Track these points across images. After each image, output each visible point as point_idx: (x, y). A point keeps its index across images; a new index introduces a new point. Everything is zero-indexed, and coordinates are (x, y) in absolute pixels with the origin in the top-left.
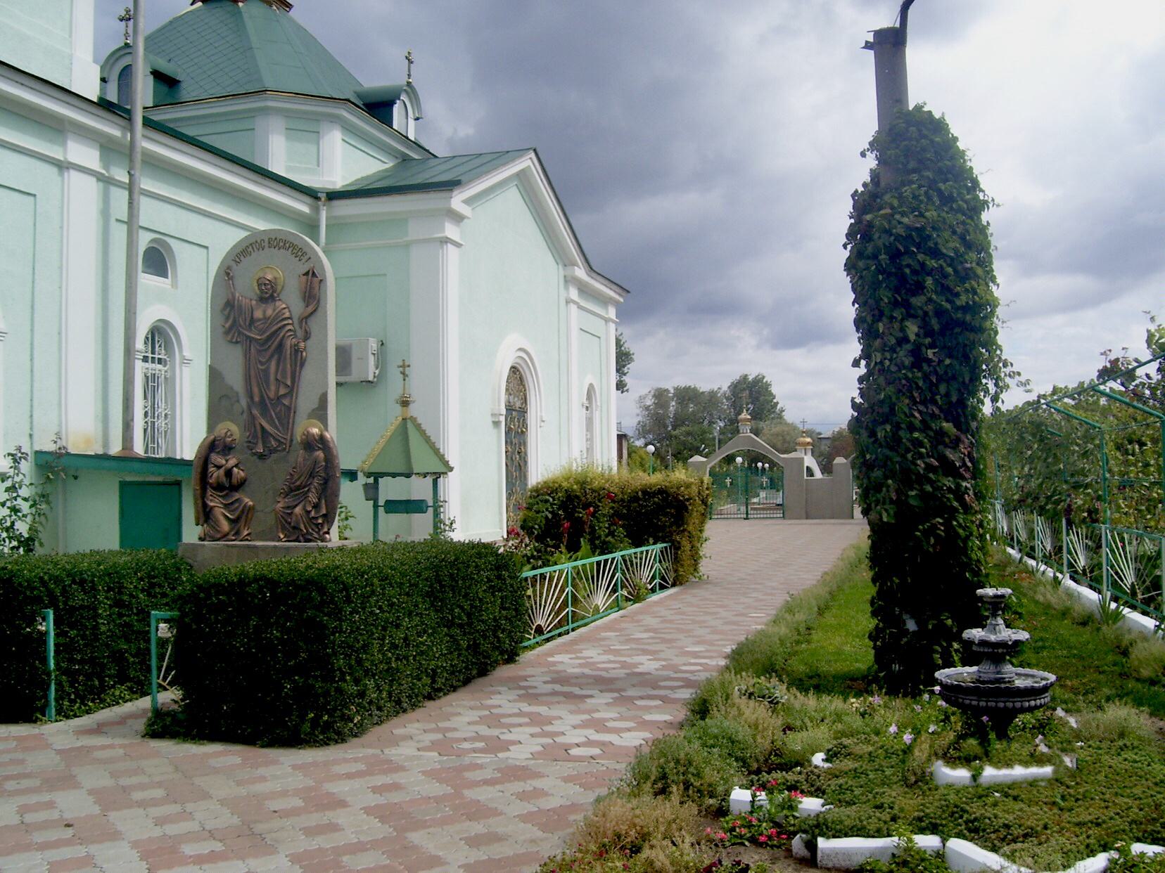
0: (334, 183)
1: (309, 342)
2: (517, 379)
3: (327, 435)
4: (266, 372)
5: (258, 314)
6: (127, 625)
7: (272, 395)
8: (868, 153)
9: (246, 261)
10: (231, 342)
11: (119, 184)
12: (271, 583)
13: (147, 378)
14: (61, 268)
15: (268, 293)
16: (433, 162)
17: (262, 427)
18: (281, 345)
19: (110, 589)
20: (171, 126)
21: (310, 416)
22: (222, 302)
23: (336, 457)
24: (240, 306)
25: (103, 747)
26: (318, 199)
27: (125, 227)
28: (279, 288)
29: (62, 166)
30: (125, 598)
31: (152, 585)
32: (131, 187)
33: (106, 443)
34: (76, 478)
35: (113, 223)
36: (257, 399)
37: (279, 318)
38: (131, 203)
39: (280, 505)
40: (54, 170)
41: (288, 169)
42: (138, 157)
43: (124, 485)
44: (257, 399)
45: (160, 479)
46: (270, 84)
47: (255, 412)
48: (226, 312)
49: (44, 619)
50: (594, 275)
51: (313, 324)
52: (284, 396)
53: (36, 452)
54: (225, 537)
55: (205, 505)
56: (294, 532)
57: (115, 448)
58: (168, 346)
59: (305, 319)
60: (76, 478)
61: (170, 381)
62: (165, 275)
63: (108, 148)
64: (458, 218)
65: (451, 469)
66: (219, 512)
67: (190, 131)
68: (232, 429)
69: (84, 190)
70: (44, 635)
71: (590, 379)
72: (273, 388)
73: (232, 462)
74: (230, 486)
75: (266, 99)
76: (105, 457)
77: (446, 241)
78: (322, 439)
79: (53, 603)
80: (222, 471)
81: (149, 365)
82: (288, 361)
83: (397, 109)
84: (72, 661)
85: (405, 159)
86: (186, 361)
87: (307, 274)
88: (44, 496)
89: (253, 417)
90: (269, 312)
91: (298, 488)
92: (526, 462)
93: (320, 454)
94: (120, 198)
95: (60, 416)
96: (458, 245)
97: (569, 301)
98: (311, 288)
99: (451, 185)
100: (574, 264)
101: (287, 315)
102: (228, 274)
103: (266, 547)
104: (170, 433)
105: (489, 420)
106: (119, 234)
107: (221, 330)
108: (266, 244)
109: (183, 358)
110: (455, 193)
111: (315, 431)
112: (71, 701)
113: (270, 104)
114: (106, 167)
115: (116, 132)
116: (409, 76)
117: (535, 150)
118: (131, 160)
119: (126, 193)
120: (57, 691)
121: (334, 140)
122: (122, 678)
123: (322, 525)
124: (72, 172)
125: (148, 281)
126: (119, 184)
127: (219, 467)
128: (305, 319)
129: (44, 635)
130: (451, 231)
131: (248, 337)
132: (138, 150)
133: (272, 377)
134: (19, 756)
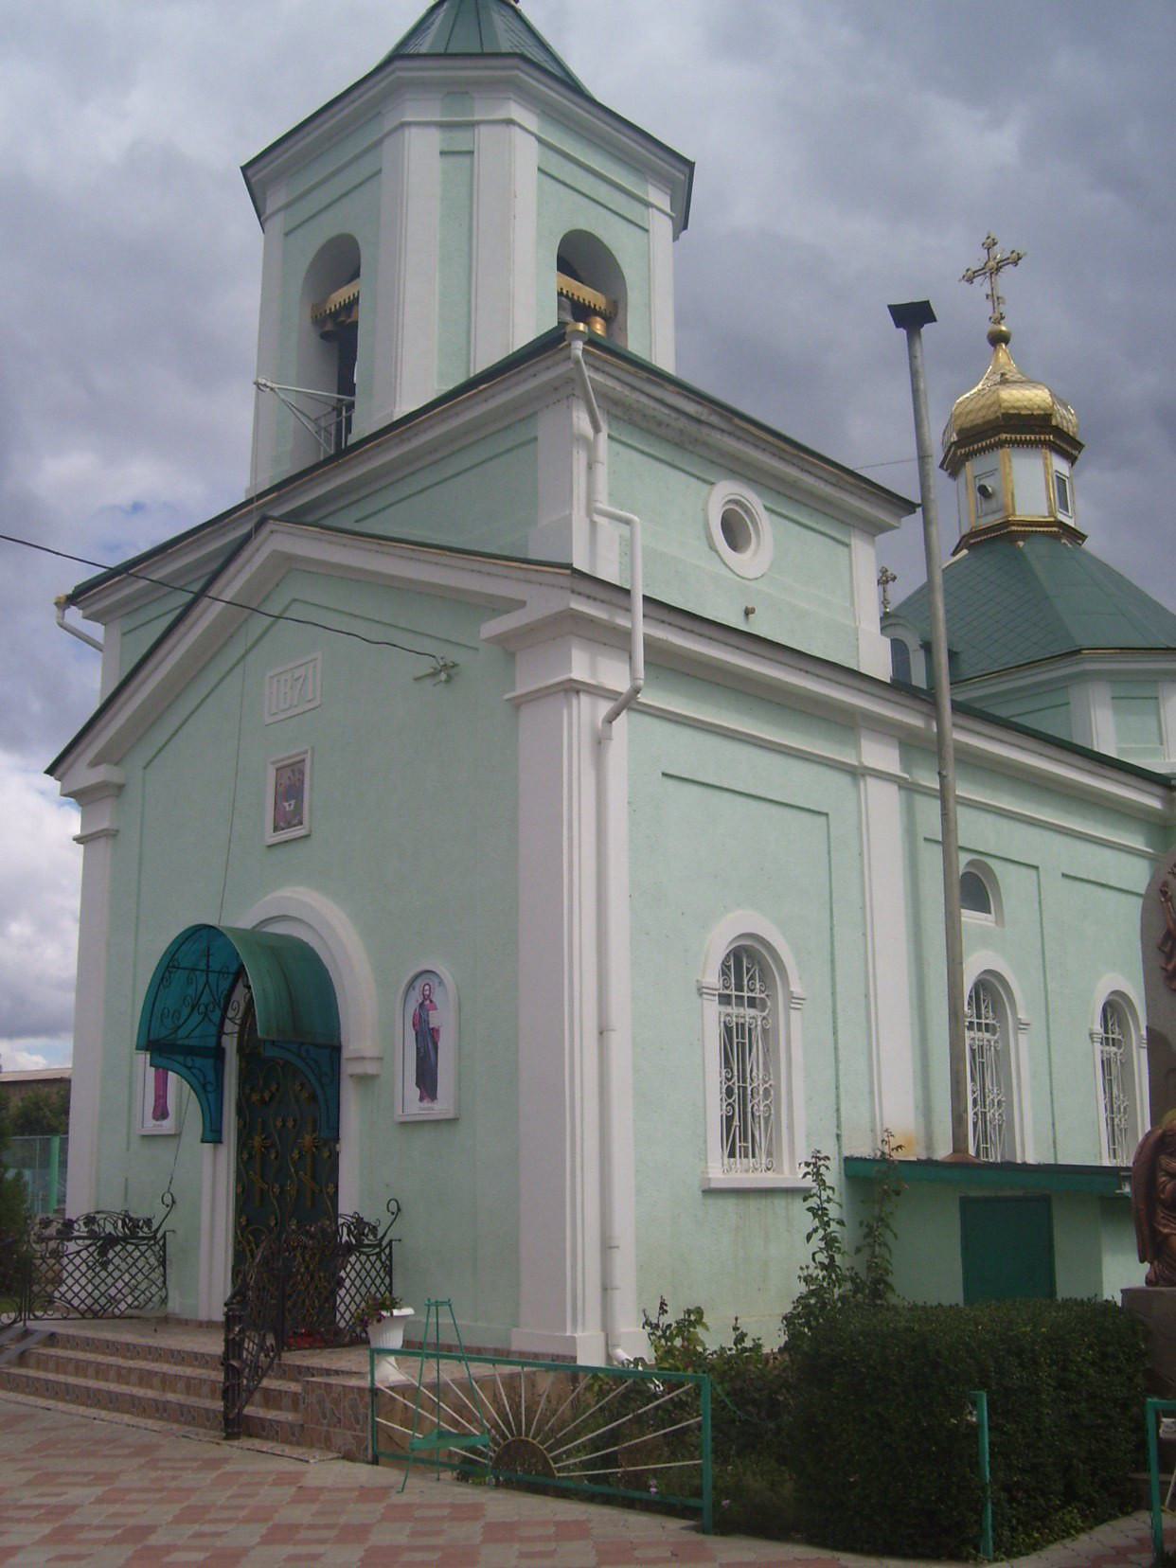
11: (926, 792)
13: (728, 1030)
14: (863, 908)
20: (977, 706)
27: (938, 850)
29: (857, 773)
30: (1073, 1376)
32: (943, 795)
33: (929, 1146)
35: (921, 843)
40: (843, 780)
41: (1120, 750)
42: (950, 754)
43: (966, 1204)
45: (1019, 1193)
46: (1082, 640)
49: (974, 1404)
53: (847, 1160)
57: (943, 1151)
61: (1002, 1056)
62: (986, 909)
63: (909, 744)
67: (1002, 712)
69: (883, 802)
76: (929, 1163)
79: (984, 1385)
81: (733, 1010)
86: (1021, 1026)
94: (930, 812)
95: (873, 1109)
104: (1006, 1126)
106: (932, 859)
109: (1018, 1022)
112: (1013, 1529)
113: (1089, 666)
114: (906, 768)
115: (916, 721)
120: (994, 1513)
124: (870, 781)
125: (969, 917)
126: (926, 792)
129: (974, 1430)
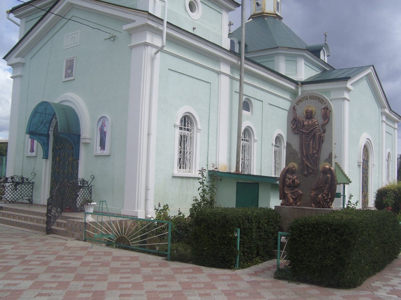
0: (302, 79)
1: (325, 134)
2: (366, 149)
3: (332, 168)
4: (309, 144)
5: (306, 123)
6: (261, 235)
7: (311, 153)
8: (248, 91)
9: (301, 104)
10: (295, 133)
11: (236, 79)
12: (331, 225)
15: (309, 115)
16: (334, 71)
17: (307, 165)
18: (315, 135)
19: (256, 222)
20: (252, 59)
21: (325, 161)
22: (292, 119)
23: (336, 177)
24: (299, 121)
25: (222, 275)
26: (298, 84)
27: (238, 95)
28: (314, 114)
29: (219, 73)
31: (269, 221)
32: (240, 81)
33: (230, 169)
34: (221, 180)
36: (305, 154)
37: (314, 124)
38: (240, 86)
39: (313, 194)
42: (243, 70)
43: (238, 183)
44: (305, 154)
45: (251, 182)
47: (304, 159)
48: (293, 123)
49: (237, 232)
50: (392, 112)
51: (327, 127)
52: (316, 153)
53: (209, 171)
54: (291, 204)
55: (284, 193)
56: (318, 204)
57: (233, 170)
58: (250, 136)
59: (323, 125)
60: (221, 180)
61: (250, 147)
63: (233, 67)
64: (349, 90)
65: (351, 182)
66: (289, 195)
67: (258, 61)
68: (294, 165)
69: (225, 81)
70: (237, 237)
71: (389, 150)
72: (311, 150)
73: (295, 177)
74: (293, 186)
75: (278, 50)
76: (230, 173)
77: (345, 99)
78: (330, 170)
79: (239, 227)
80: (291, 180)
82: (317, 141)
83: (322, 52)
84: (244, 247)
85: (324, 71)
86: (255, 141)
87: (325, 109)
88: (213, 186)
89: (303, 161)
90: (310, 123)
91: (320, 188)
92: (368, 180)
93: (329, 175)
94: (237, 85)
96: (348, 100)
97: (383, 121)
98: (326, 114)
99: (347, 79)
100: (385, 108)
101: (317, 123)
102: (294, 109)
103: (309, 209)
104: (249, 166)
105: (357, 164)
106: (237, 96)
107: (291, 129)
108: (309, 97)
109: (254, 139)
110: (349, 81)
111: (327, 167)
112: (244, 262)
113: (280, 52)
116: (326, 41)
117: (373, 66)
118: (241, 71)
119: (238, 83)
121: (302, 64)
122: (258, 254)
123: (329, 202)
124: (222, 75)
125: (244, 112)
126: (236, 79)
127: (290, 179)
128: (323, 125)
130: (346, 95)
131: (301, 131)
132: (243, 67)
133: (311, 146)
134: (159, 268)
